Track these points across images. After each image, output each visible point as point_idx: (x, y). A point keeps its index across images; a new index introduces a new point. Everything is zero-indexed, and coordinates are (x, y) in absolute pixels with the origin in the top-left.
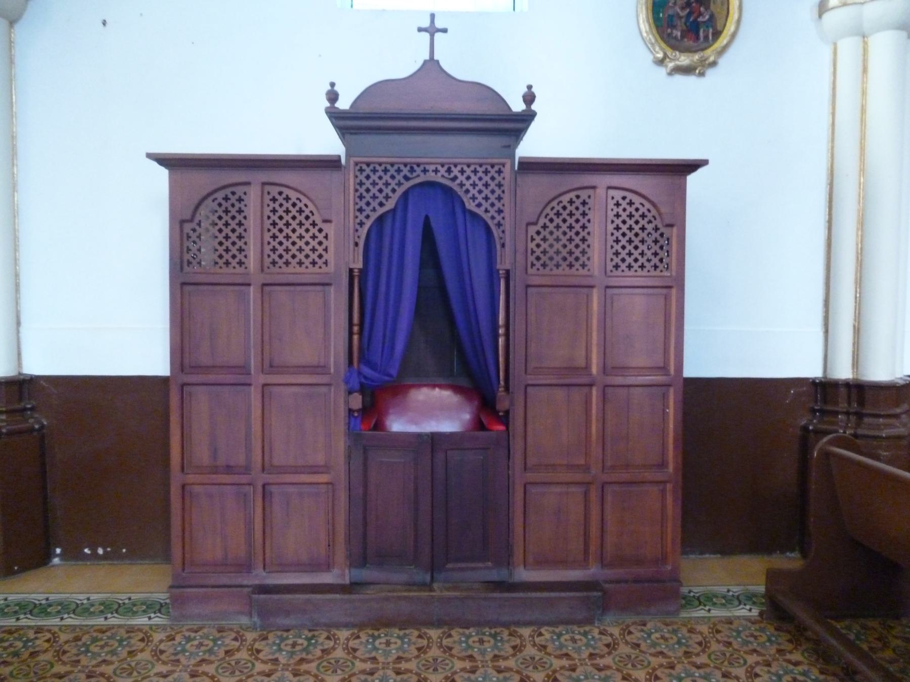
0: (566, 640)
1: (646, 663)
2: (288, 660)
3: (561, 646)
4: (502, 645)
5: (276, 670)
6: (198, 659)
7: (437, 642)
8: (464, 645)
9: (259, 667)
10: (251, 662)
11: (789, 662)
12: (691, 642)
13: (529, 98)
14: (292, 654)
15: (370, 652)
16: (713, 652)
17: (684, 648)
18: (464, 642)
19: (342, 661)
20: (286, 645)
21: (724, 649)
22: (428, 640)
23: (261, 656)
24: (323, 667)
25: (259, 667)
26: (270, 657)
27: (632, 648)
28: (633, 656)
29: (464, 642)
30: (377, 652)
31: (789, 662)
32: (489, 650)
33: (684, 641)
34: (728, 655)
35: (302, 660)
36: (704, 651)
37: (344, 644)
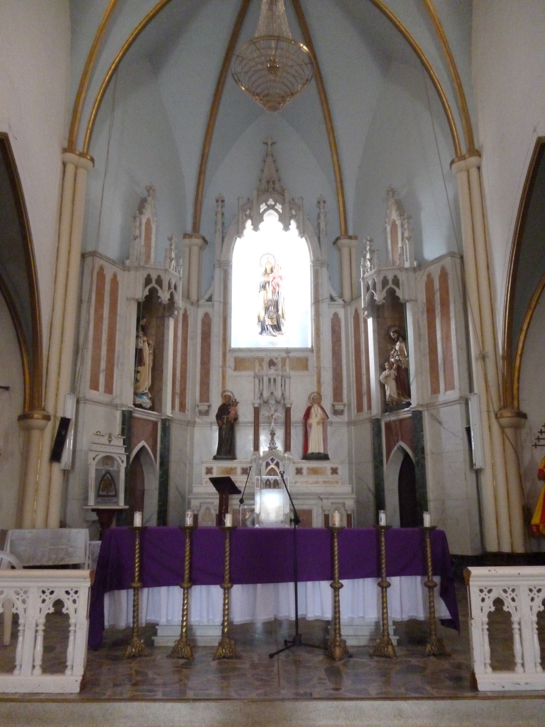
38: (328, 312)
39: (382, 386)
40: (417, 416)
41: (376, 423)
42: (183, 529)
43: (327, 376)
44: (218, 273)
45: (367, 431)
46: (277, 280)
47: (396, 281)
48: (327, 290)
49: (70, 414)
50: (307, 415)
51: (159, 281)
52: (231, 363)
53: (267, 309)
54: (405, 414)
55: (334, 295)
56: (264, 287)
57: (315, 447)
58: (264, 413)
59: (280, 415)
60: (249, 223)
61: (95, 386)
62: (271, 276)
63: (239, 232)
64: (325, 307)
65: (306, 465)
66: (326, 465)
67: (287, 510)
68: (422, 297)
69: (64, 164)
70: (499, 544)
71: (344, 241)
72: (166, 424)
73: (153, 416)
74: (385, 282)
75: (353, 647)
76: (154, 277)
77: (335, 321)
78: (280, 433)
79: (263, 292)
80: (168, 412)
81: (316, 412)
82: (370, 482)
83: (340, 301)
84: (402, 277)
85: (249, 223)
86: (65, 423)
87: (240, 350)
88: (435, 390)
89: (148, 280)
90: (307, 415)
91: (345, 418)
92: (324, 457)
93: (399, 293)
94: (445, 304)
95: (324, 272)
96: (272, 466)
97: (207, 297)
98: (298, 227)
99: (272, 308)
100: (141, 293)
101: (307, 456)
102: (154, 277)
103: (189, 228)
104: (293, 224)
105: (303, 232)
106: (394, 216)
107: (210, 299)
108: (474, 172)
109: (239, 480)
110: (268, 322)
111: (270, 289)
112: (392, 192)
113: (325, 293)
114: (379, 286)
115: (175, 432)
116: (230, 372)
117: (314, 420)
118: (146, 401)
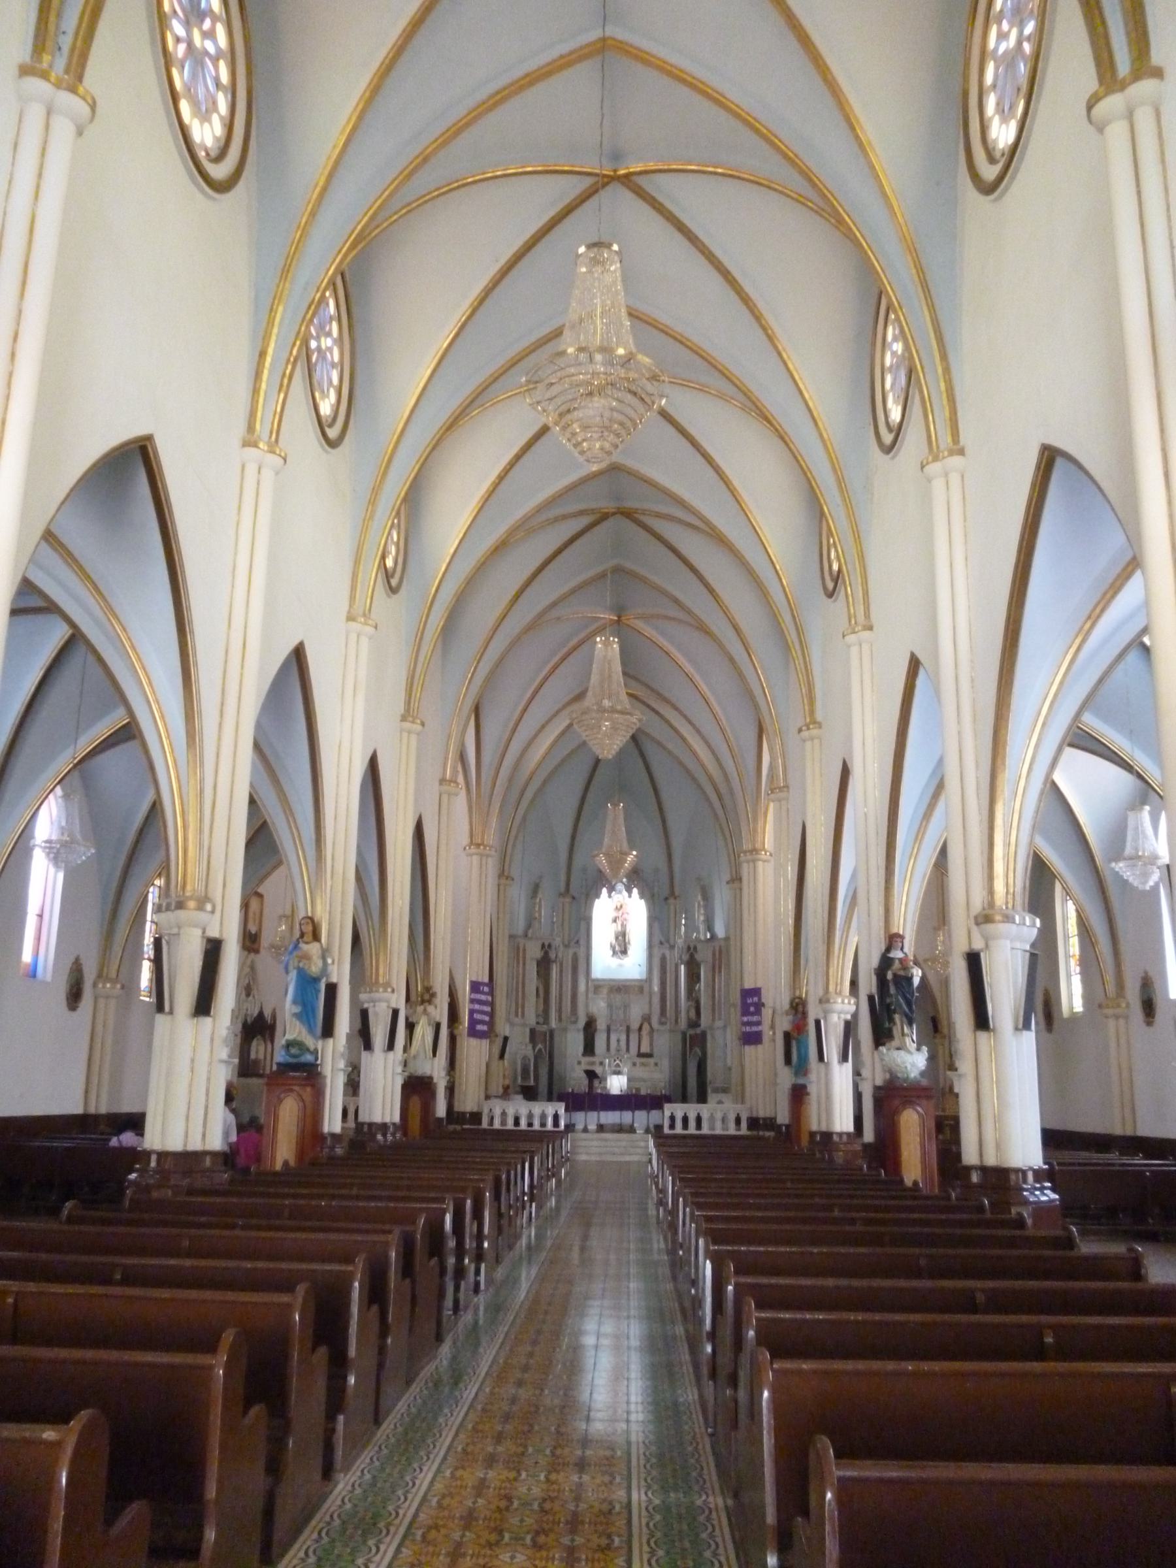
38: (657, 953)
39: (688, 1012)
40: (704, 1034)
41: (684, 1034)
42: (568, 1093)
43: (656, 1000)
44: (583, 925)
45: (680, 1037)
46: (625, 916)
47: (695, 948)
48: (658, 937)
49: (507, 1034)
50: (640, 1029)
51: (550, 946)
52: (591, 989)
53: (617, 938)
54: (698, 1031)
55: (663, 940)
56: (615, 921)
57: (645, 1049)
58: (613, 1028)
59: (624, 1028)
60: (604, 890)
61: (517, 1015)
62: (621, 912)
63: (598, 896)
64: (656, 951)
65: (639, 1061)
66: (651, 1061)
67: (31, 968)
68: (710, 959)
69: (499, 885)
70: (981, 1155)
71: (671, 901)
72: (552, 1032)
73: (544, 1028)
74: (689, 948)
75: (566, 1038)
76: (546, 944)
77: (663, 960)
78: (623, 1037)
79: (614, 924)
80: (553, 1024)
81: (646, 1027)
82: (679, 1071)
83: (667, 945)
84: (699, 947)
85: (604, 890)
86: (506, 1039)
87: (598, 980)
88: (713, 1020)
89: (543, 946)
90: (640, 1029)
91: (668, 1027)
92: (649, 1055)
93: (696, 956)
94: (720, 968)
95: (656, 925)
96: (618, 1062)
97: (575, 941)
98: (639, 893)
99: (620, 938)
100: (538, 954)
101: (640, 1055)
102: (546, 944)
103: (562, 889)
104: (635, 891)
105: (642, 896)
106: (699, 898)
107: (577, 942)
108: (738, 892)
109: (598, 1070)
110: (617, 948)
111: (619, 923)
112: (699, 879)
113: (656, 940)
114: (685, 950)
115: (557, 1039)
116: (590, 995)
117: (645, 1032)
118: (541, 1020)
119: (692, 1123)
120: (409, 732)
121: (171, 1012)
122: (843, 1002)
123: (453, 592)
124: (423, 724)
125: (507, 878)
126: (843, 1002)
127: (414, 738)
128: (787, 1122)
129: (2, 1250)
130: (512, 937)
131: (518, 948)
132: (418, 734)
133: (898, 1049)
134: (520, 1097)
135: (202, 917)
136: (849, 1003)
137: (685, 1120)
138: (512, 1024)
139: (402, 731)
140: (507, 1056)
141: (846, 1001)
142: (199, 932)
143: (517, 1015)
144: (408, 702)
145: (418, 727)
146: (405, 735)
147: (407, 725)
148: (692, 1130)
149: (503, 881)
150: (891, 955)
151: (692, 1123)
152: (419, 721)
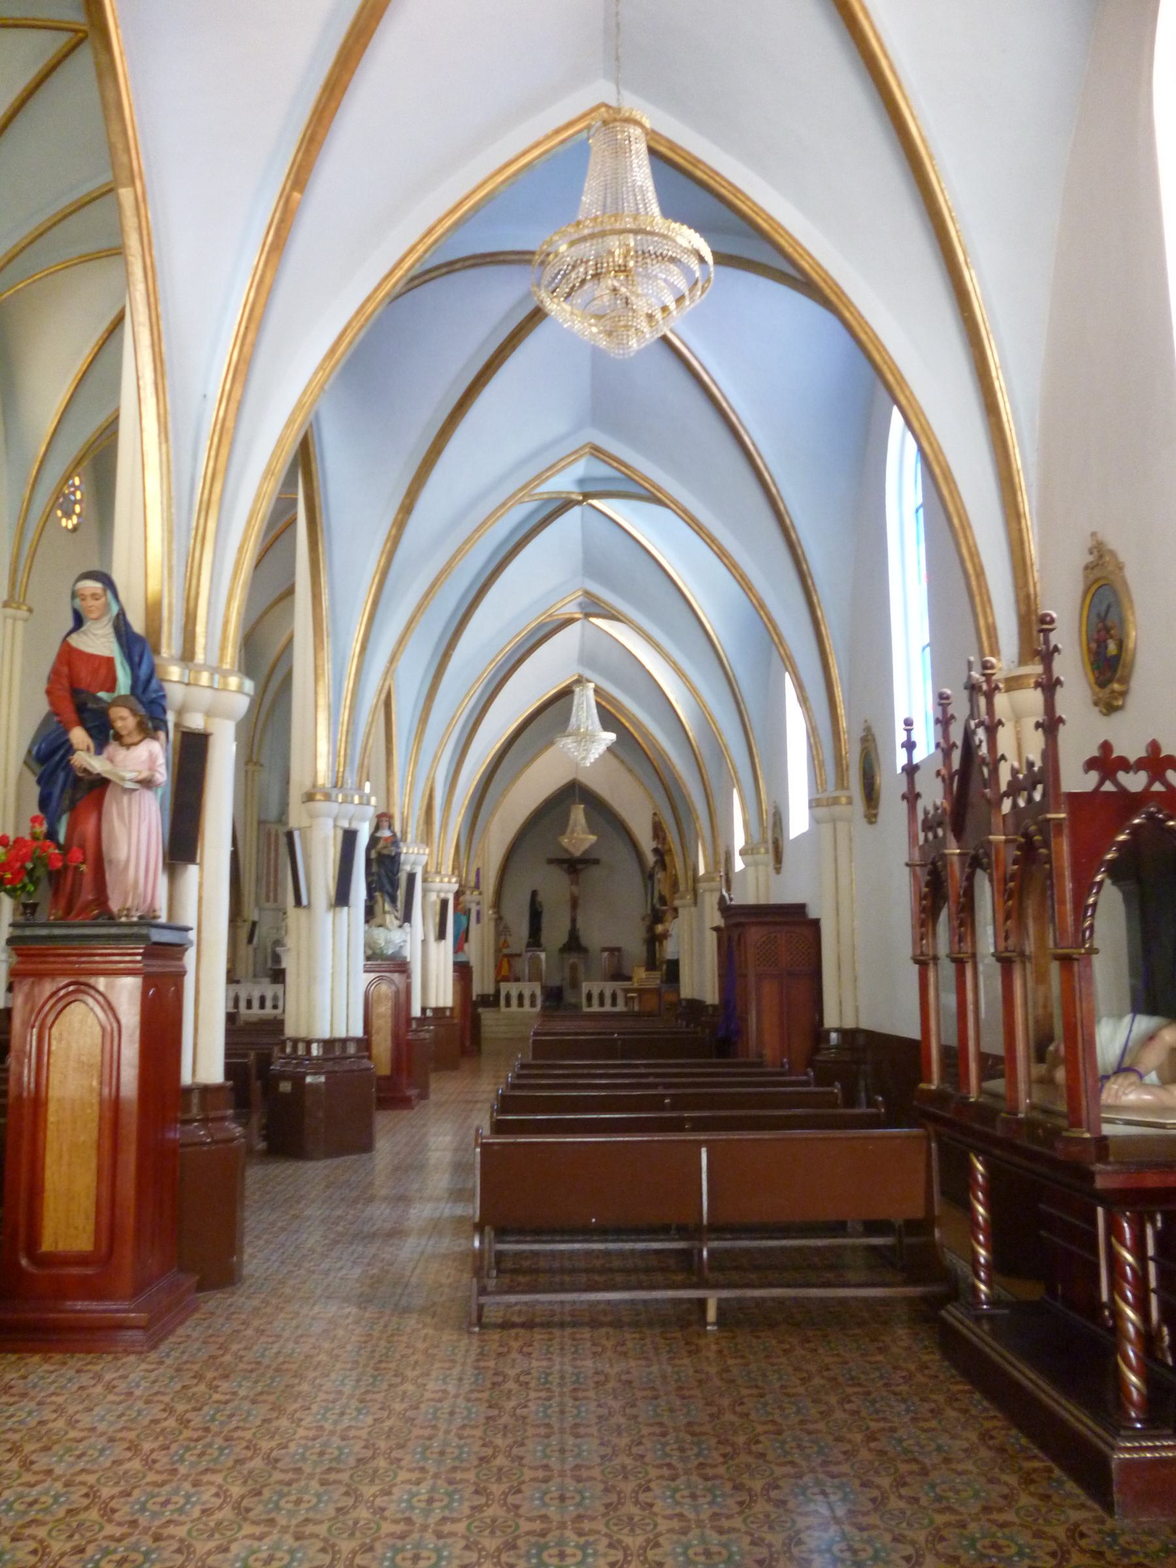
0: (864, 1550)
1: (1022, 1513)
2: (562, 1535)
3: (870, 1541)
4: (674, 1549)
5: (297, 1526)
6: (124, 1543)
7: (632, 1555)
8: (590, 1551)
9: (322, 1530)
10: (789, 1529)
11: (954, 1471)
12: (1039, 1553)
13: (924, 649)
14: (417, 1546)
15: (445, 1546)
16: (1064, 1523)
17: (966, 1533)
18: (680, 1555)
19: (345, 1535)
20: (429, 1558)
21: (1046, 1529)
22: (646, 1558)
23: (320, 1544)
24: (510, 1527)
25: (322, 1530)
26: (306, 1542)
27: (904, 1537)
28: (904, 1525)
29: (680, 1555)
30: (436, 1545)
31: (954, 1471)
32: (695, 1542)
33: (1027, 1550)
34: (1041, 1521)
35: (402, 1537)
36: (938, 1529)
37: (347, 1558)
49: (256, 918)
69: (246, 771)
86: (254, 924)
119: (608, 1001)
120: (15, 619)
121: (309, 906)
122: (441, 881)
123: (62, 473)
124: (30, 610)
125: (255, 764)
126: (441, 881)
127: (20, 625)
128: (716, 1001)
129: (1175, 1136)
130: (261, 822)
131: (269, 835)
132: (26, 620)
133: (380, 926)
134: (267, 980)
135: (334, 807)
136: (449, 882)
137: (262, 1000)
138: (261, 909)
139: (5, 618)
140: (255, 940)
141: (446, 880)
142: (330, 822)
143: (268, 900)
144: (13, 584)
145: (23, 613)
146: (9, 622)
147: (10, 611)
148: (608, 1008)
149: (250, 767)
150: (378, 834)
151: (608, 1001)
152: (25, 608)
